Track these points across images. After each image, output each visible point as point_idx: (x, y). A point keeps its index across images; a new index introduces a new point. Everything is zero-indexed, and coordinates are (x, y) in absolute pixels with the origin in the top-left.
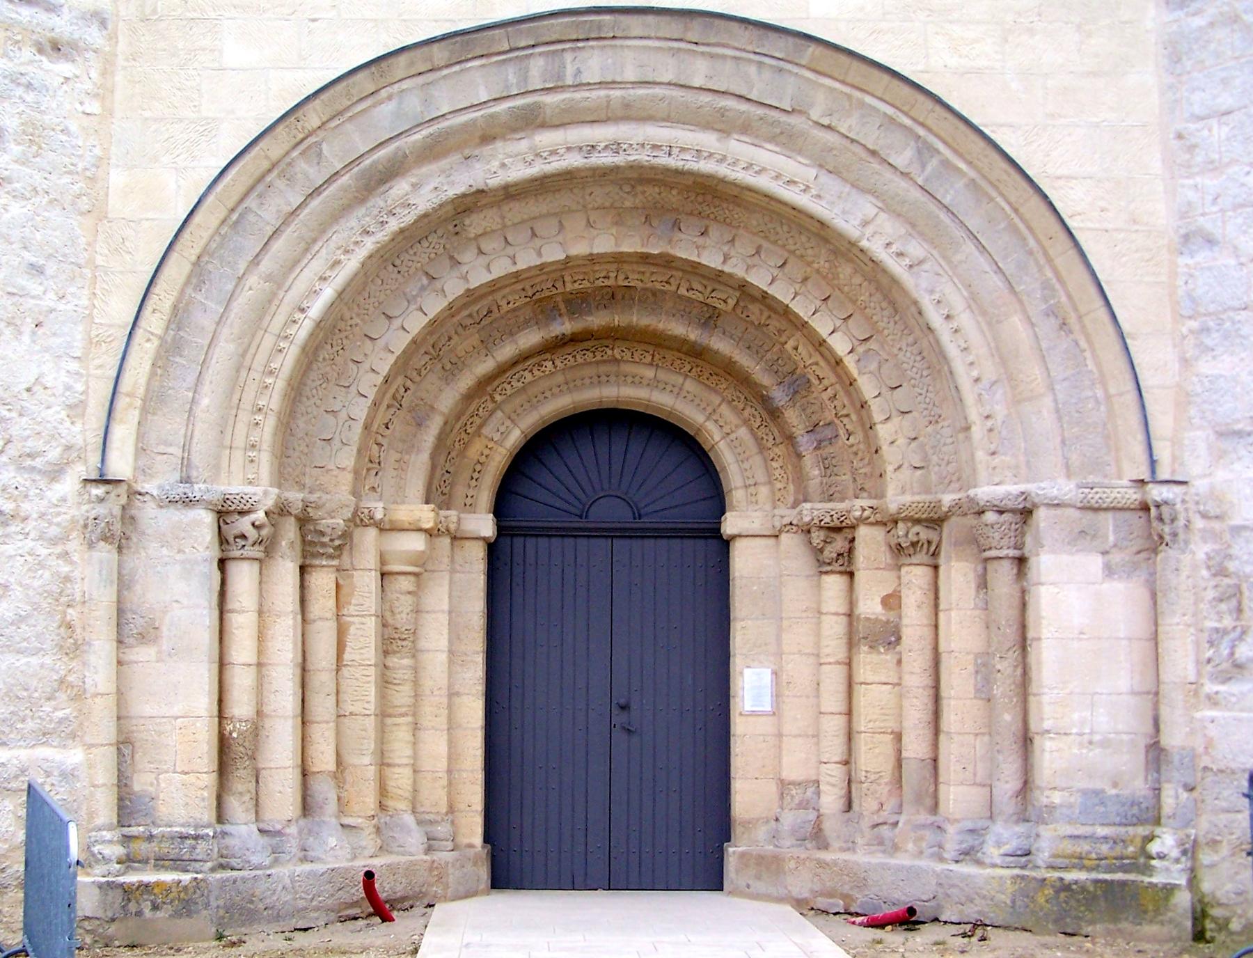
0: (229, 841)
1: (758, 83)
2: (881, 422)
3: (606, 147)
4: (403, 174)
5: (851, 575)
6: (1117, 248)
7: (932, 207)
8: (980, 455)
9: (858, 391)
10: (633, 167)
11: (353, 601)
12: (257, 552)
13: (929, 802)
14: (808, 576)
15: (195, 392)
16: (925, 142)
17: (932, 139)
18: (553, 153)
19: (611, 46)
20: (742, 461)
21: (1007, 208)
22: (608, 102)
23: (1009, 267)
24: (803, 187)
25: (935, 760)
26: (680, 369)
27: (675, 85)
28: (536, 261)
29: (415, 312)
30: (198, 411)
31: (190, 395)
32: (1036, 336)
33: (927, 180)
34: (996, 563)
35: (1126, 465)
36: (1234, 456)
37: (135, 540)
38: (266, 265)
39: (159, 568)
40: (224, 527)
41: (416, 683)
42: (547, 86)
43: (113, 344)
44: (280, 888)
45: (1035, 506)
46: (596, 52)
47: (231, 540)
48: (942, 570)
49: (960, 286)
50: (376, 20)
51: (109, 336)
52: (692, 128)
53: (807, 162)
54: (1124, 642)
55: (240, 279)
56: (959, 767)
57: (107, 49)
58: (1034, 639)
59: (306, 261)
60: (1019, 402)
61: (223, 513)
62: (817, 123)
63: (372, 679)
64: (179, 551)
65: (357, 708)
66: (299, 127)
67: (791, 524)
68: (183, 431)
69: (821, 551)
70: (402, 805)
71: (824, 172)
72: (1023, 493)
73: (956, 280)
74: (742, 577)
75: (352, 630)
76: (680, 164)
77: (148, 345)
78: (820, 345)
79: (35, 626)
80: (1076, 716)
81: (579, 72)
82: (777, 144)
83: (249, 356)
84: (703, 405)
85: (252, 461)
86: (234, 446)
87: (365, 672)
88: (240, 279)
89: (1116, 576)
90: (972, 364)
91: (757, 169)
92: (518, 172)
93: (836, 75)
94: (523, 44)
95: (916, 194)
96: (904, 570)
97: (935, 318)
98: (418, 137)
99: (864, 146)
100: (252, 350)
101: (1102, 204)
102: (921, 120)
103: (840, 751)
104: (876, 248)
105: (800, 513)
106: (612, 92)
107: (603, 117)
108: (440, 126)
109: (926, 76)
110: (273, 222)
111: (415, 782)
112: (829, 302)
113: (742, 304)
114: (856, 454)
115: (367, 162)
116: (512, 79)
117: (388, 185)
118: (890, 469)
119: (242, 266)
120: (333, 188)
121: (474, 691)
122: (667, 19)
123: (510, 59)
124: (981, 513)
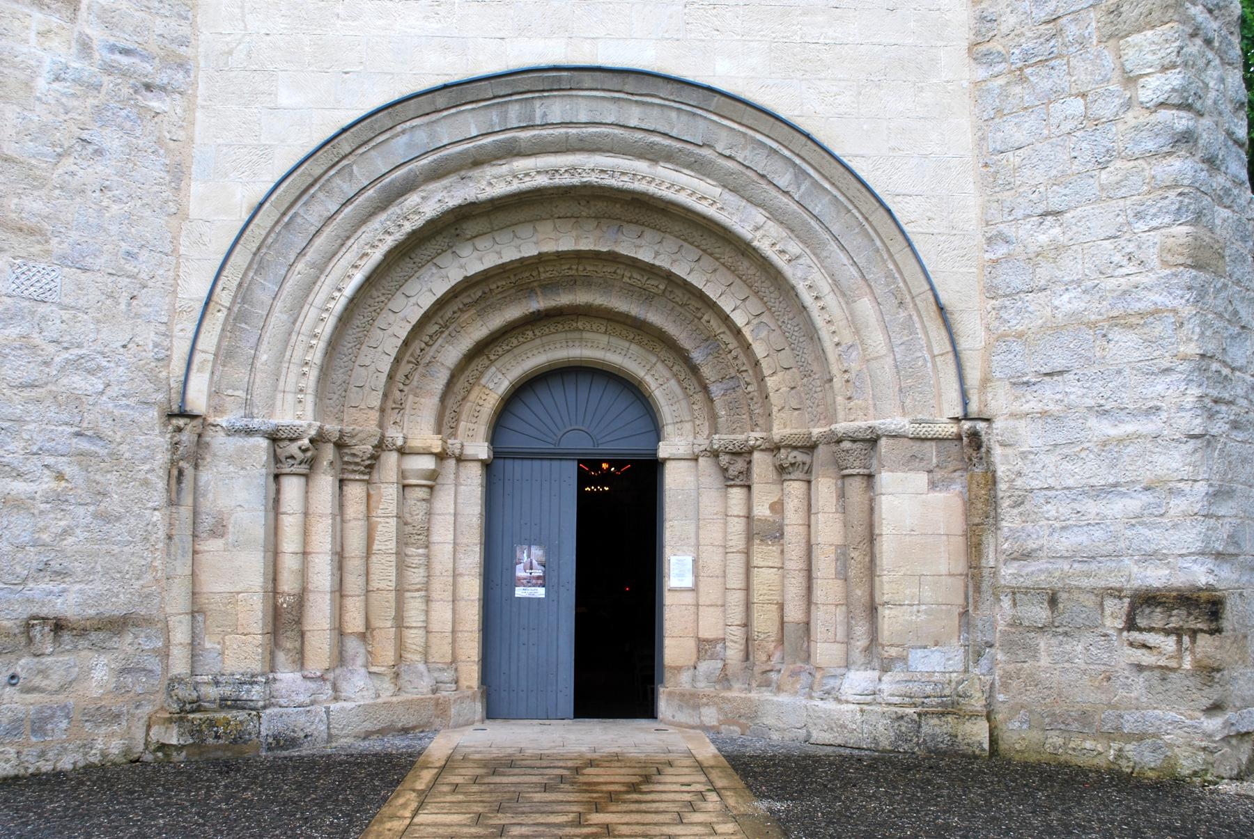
0: (277, 685)
1: (678, 124)
3: (566, 171)
4: (415, 189)
5: (749, 487)
7: (805, 216)
8: (840, 399)
9: (753, 353)
10: (586, 186)
11: (381, 507)
12: (303, 469)
13: (803, 655)
14: (718, 489)
16: (800, 168)
17: (805, 166)
18: (527, 175)
21: (860, 217)
22: (567, 138)
23: (861, 262)
25: (808, 623)
27: (616, 125)
28: (517, 256)
30: (258, 364)
31: (253, 352)
33: (801, 197)
35: (945, 406)
36: (1024, 400)
37: (208, 460)
38: (311, 255)
40: (279, 450)
41: (428, 566)
44: (317, 719)
45: (879, 437)
46: (557, 100)
47: (283, 460)
53: (714, 183)
54: (945, 538)
55: (291, 266)
56: (824, 629)
57: (190, 92)
58: (878, 535)
60: (868, 361)
61: (274, 438)
62: (721, 154)
63: (394, 564)
65: (382, 585)
68: (247, 379)
69: (726, 470)
70: (417, 657)
74: (670, 489)
75: (380, 528)
77: (219, 314)
78: (726, 319)
80: (908, 592)
81: (545, 115)
82: (692, 170)
83: (298, 324)
84: (643, 364)
85: (300, 402)
87: (388, 559)
88: (291, 266)
90: (834, 332)
91: (677, 188)
92: (500, 189)
93: (735, 118)
94: (502, 93)
95: (795, 207)
97: (807, 298)
98: (425, 161)
100: (301, 319)
101: (929, 214)
103: (740, 616)
104: (764, 246)
105: (711, 442)
106: (570, 130)
107: (564, 148)
108: (442, 154)
109: (799, 119)
110: (316, 224)
111: (427, 639)
112: (732, 287)
113: (669, 289)
114: (752, 399)
115: (387, 180)
116: (495, 119)
117: (404, 198)
118: (775, 409)
119: (292, 257)
120: (361, 199)
121: (473, 573)
122: (611, 75)
123: (493, 105)
124: (839, 441)
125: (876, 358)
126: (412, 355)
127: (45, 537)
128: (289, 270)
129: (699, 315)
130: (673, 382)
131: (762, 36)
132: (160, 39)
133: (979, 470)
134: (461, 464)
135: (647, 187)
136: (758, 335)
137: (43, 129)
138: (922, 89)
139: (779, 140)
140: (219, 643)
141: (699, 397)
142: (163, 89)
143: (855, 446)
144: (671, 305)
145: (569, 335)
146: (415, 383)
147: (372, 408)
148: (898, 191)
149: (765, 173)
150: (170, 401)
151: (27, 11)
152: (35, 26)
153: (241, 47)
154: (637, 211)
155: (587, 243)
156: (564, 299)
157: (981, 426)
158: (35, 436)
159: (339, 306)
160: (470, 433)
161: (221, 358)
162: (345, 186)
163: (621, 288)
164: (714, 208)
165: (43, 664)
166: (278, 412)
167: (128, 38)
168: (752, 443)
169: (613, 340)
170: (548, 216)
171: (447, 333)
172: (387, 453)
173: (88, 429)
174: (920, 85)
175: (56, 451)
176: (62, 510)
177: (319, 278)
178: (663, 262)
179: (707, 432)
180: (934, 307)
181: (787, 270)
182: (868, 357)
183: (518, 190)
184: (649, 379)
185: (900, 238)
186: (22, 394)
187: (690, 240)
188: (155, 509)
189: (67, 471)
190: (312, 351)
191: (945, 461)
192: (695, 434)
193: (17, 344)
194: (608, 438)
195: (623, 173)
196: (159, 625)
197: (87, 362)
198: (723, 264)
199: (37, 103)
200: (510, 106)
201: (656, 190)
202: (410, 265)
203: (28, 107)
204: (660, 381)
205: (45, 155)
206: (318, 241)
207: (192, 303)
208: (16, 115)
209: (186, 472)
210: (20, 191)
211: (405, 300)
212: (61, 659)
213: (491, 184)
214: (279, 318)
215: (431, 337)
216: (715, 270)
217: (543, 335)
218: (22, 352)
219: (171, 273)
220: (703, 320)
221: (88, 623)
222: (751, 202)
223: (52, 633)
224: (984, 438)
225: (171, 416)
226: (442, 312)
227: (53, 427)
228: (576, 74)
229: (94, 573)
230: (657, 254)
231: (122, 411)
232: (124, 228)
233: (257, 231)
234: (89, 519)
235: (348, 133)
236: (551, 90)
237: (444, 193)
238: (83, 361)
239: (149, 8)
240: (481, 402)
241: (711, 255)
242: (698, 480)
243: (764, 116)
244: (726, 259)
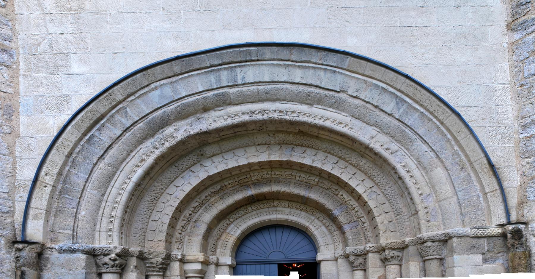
2: (377, 216)
3: (259, 112)
6: (491, 134)
7: (402, 127)
15: (77, 209)
18: (236, 115)
19: (257, 64)
20: (323, 237)
21: (438, 123)
22: (258, 92)
24: (345, 125)
26: (299, 208)
29: (187, 185)
31: (75, 210)
32: (449, 175)
33: (400, 116)
34: (430, 262)
35: (494, 219)
37: (49, 266)
40: (98, 261)
42: (230, 84)
43: (27, 188)
46: (251, 68)
48: (403, 267)
49: (413, 159)
50: (144, 53)
52: (296, 103)
57: (14, 67)
59: (129, 160)
62: (351, 96)
64: (70, 270)
67: (341, 255)
68: (72, 224)
69: (353, 263)
71: (354, 119)
72: (444, 234)
73: (411, 157)
76: (291, 118)
81: (243, 78)
82: (333, 108)
83: (106, 196)
86: (101, 230)
89: (488, 263)
90: (419, 188)
91: (324, 118)
92: (221, 123)
93: (360, 72)
96: (387, 267)
97: (402, 172)
99: (372, 104)
100: (107, 194)
102: (399, 88)
104: (377, 147)
106: (259, 87)
112: (356, 175)
114: (366, 230)
115: (151, 117)
116: (213, 81)
117: (164, 129)
118: (381, 232)
122: (281, 48)
125: (445, 199)
126: (184, 217)
128: (93, 167)
129: (337, 193)
130: (323, 228)
131: (376, 24)
133: (520, 250)
134: (219, 267)
135: (308, 119)
136: (370, 197)
138: (477, 49)
139: (388, 82)
141: (337, 233)
143: (434, 244)
144: (321, 189)
145: (270, 209)
146: (188, 230)
147: (161, 241)
148: (463, 105)
149: (378, 104)
153: (45, 41)
154: (302, 138)
155: (275, 156)
156: (265, 189)
157: (521, 227)
159: (130, 186)
160: (223, 254)
162: (124, 120)
163: (295, 183)
164: (347, 128)
166: (97, 241)
168: (368, 249)
169: (292, 210)
170: (252, 144)
171: (204, 207)
172: (174, 262)
174: (476, 47)
177: (116, 172)
178: (317, 164)
179: (341, 248)
180: (488, 166)
181: (392, 159)
182: (440, 199)
183: (231, 124)
184: (311, 227)
185: (465, 130)
187: (332, 152)
190: (115, 210)
191: (493, 248)
192: (335, 249)
194: (291, 255)
195: (293, 112)
198: (350, 164)
200: (221, 72)
201: (313, 120)
202: (175, 170)
204: (317, 227)
206: (111, 152)
207: (26, 182)
211: (176, 188)
213: (215, 121)
214: (91, 193)
215: (195, 208)
216: (346, 167)
217: (257, 209)
219: (9, 166)
220: (339, 196)
222: (369, 124)
224: (524, 233)
225: (15, 242)
226: (200, 196)
228: (260, 48)
230: (314, 161)
233: (66, 143)
235: (118, 86)
236: (246, 61)
237: (188, 127)
240: (227, 240)
241: (343, 159)
242: (337, 269)
243: (379, 67)
244: (353, 160)
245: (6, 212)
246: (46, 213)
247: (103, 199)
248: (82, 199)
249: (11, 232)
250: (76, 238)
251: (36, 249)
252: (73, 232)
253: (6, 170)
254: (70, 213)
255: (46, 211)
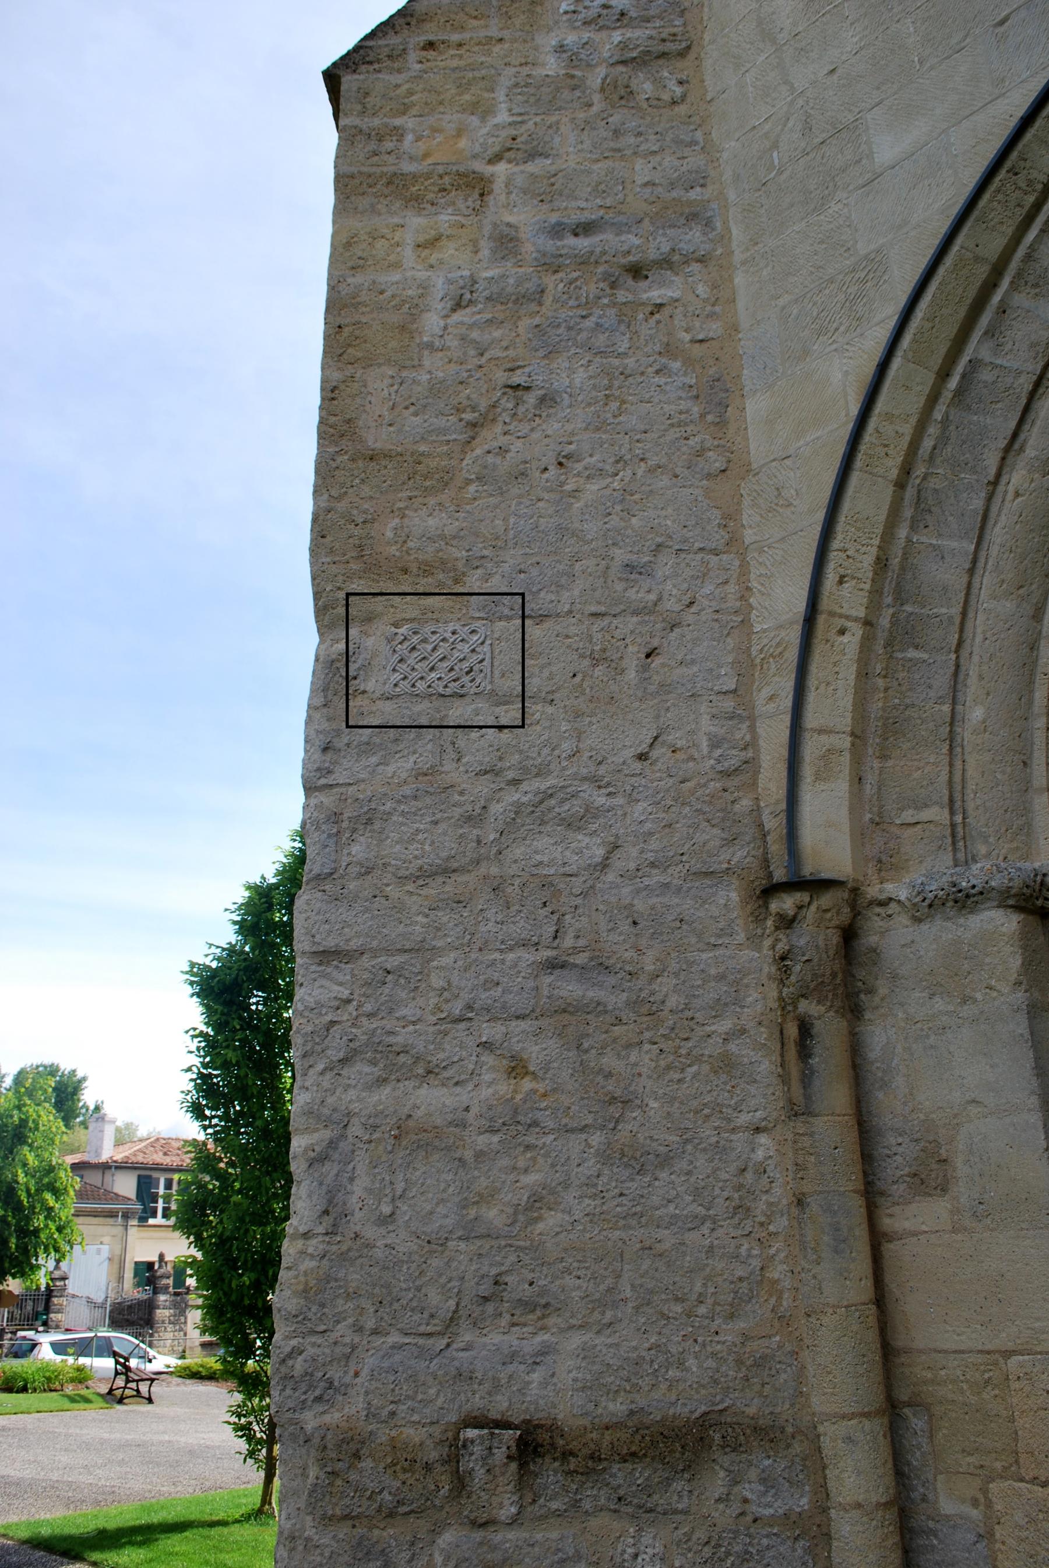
15: (954, 702)
30: (967, 735)
31: (946, 708)
37: (883, 991)
39: (932, 1040)
43: (786, 655)
51: (778, 645)
55: (995, 483)
64: (964, 1001)
66: (1023, 185)
68: (944, 777)
77: (845, 639)
79: (689, 1173)
119: (991, 461)
127: (494, 1215)
132: (648, 190)
137: (436, 389)
140: (975, 1503)
142: (666, 263)
150: (766, 862)
151: (396, 220)
152: (410, 238)
158: (455, 979)
161: (873, 741)
165: (494, 1548)
167: (583, 205)
173: (576, 950)
175: (504, 1007)
176: (528, 1147)
186: (425, 892)
188: (758, 1130)
189: (535, 1052)
193: (407, 790)
196: (797, 1448)
197: (563, 801)
199: (426, 353)
203: (408, 363)
205: (444, 431)
208: (387, 381)
209: (818, 1027)
210: (401, 505)
212: (539, 1536)
218: (419, 804)
219: (732, 588)
221: (608, 1436)
223: (514, 1466)
225: (771, 890)
227: (497, 955)
229: (615, 1305)
231: (654, 900)
232: (615, 521)
234: (591, 1166)
238: (553, 802)
239: (619, 150)
245: (736, 770)
246: (853, 745)
247: (1040, 631)
248: (964, 653)
249: (754, 848)
250: (964, 838)
251: (838, 913)
252: (952, 813)
253: (724, 606)
254: (931, 725)
255: (853, 734)
